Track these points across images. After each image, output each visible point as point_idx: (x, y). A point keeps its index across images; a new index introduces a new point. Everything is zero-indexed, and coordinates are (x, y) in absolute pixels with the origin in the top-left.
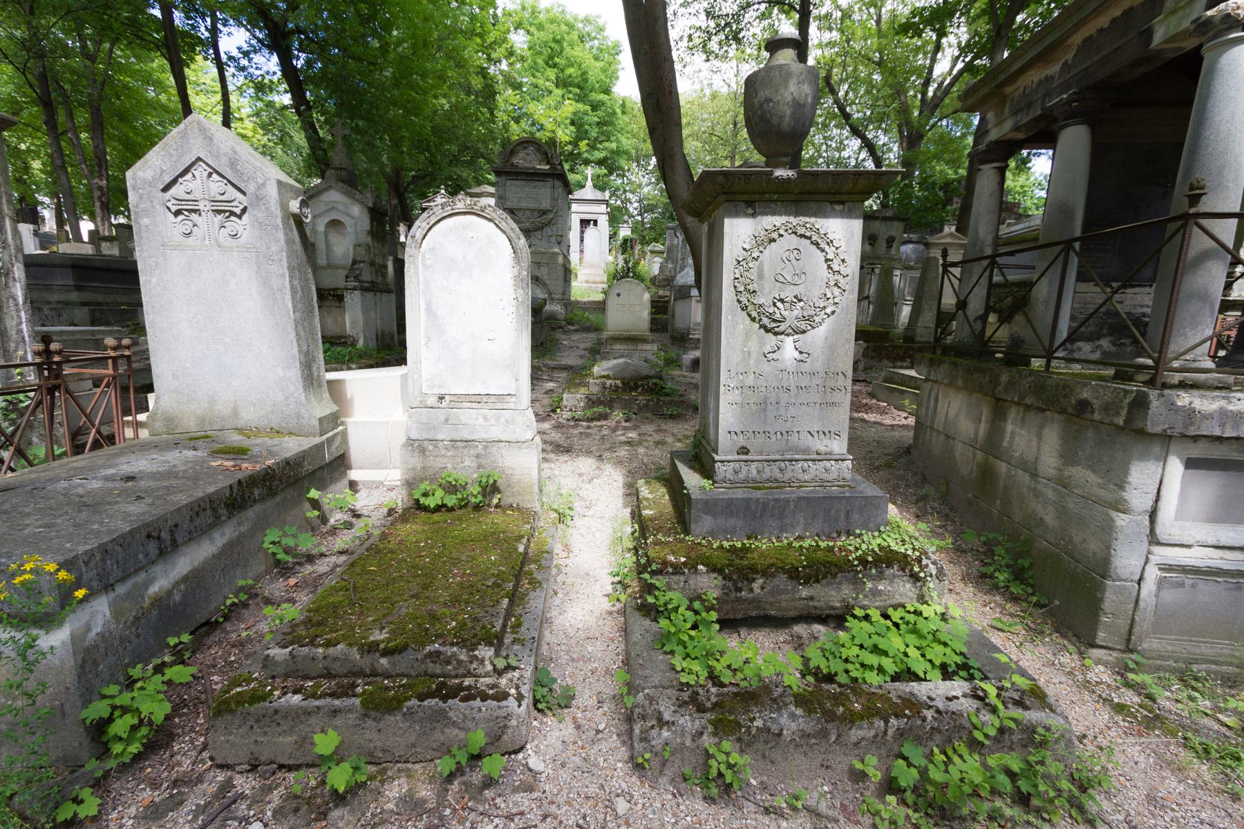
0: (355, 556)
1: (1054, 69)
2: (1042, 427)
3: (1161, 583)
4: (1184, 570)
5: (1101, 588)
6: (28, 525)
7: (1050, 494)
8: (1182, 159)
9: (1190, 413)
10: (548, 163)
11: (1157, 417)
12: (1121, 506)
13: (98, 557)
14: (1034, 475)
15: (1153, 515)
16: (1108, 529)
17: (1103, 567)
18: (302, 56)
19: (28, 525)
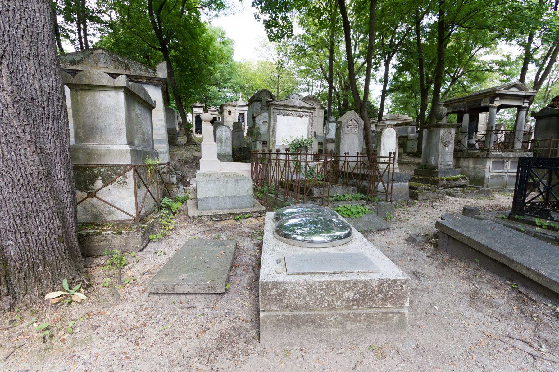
0: (182, 245)
1: (462, 104)
2: (469, 160)
3: (491, 178)
4: (494, 176)
5: (484, 180)
6: (70, 210)
7: (472, 170)
8: (423, 135)
9: (493, 155)
10: (271, 98)
11: (490, 156)
12: (485, 168)
13: (141, 222)
14: (468, 168)
15: (489, 169)
16: (484, 172)
17: (484, 177)
18: (187, 12)
19: (70, 210)
